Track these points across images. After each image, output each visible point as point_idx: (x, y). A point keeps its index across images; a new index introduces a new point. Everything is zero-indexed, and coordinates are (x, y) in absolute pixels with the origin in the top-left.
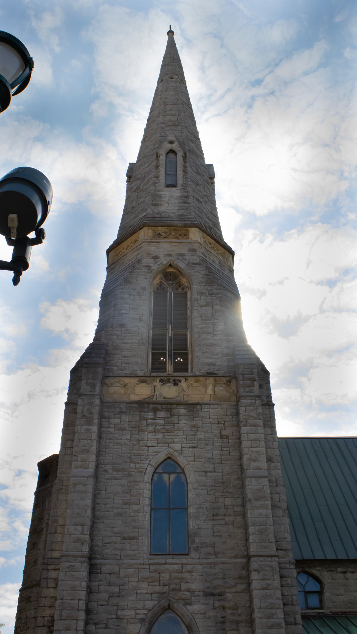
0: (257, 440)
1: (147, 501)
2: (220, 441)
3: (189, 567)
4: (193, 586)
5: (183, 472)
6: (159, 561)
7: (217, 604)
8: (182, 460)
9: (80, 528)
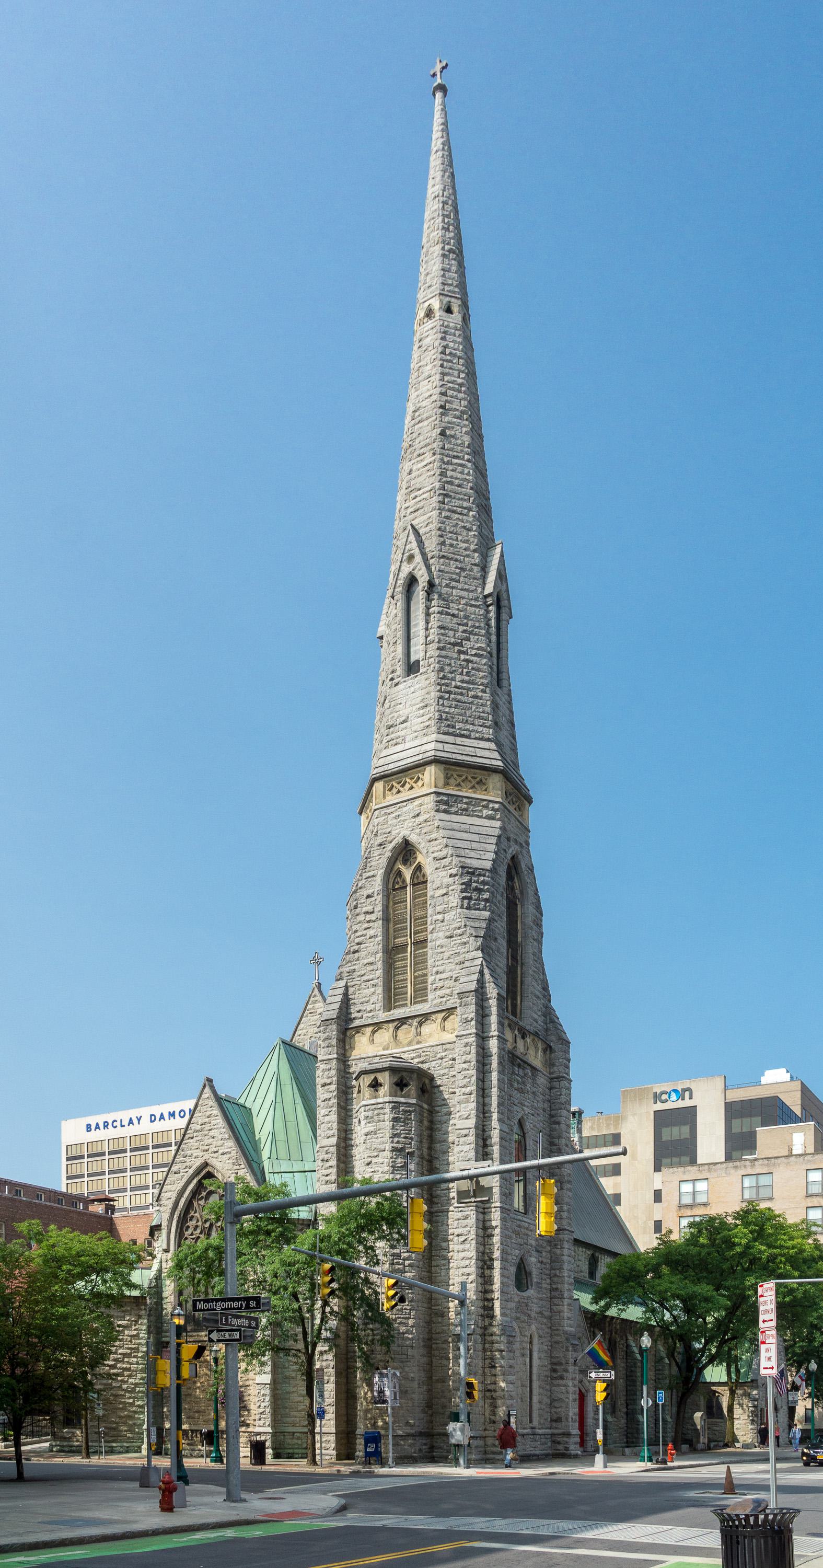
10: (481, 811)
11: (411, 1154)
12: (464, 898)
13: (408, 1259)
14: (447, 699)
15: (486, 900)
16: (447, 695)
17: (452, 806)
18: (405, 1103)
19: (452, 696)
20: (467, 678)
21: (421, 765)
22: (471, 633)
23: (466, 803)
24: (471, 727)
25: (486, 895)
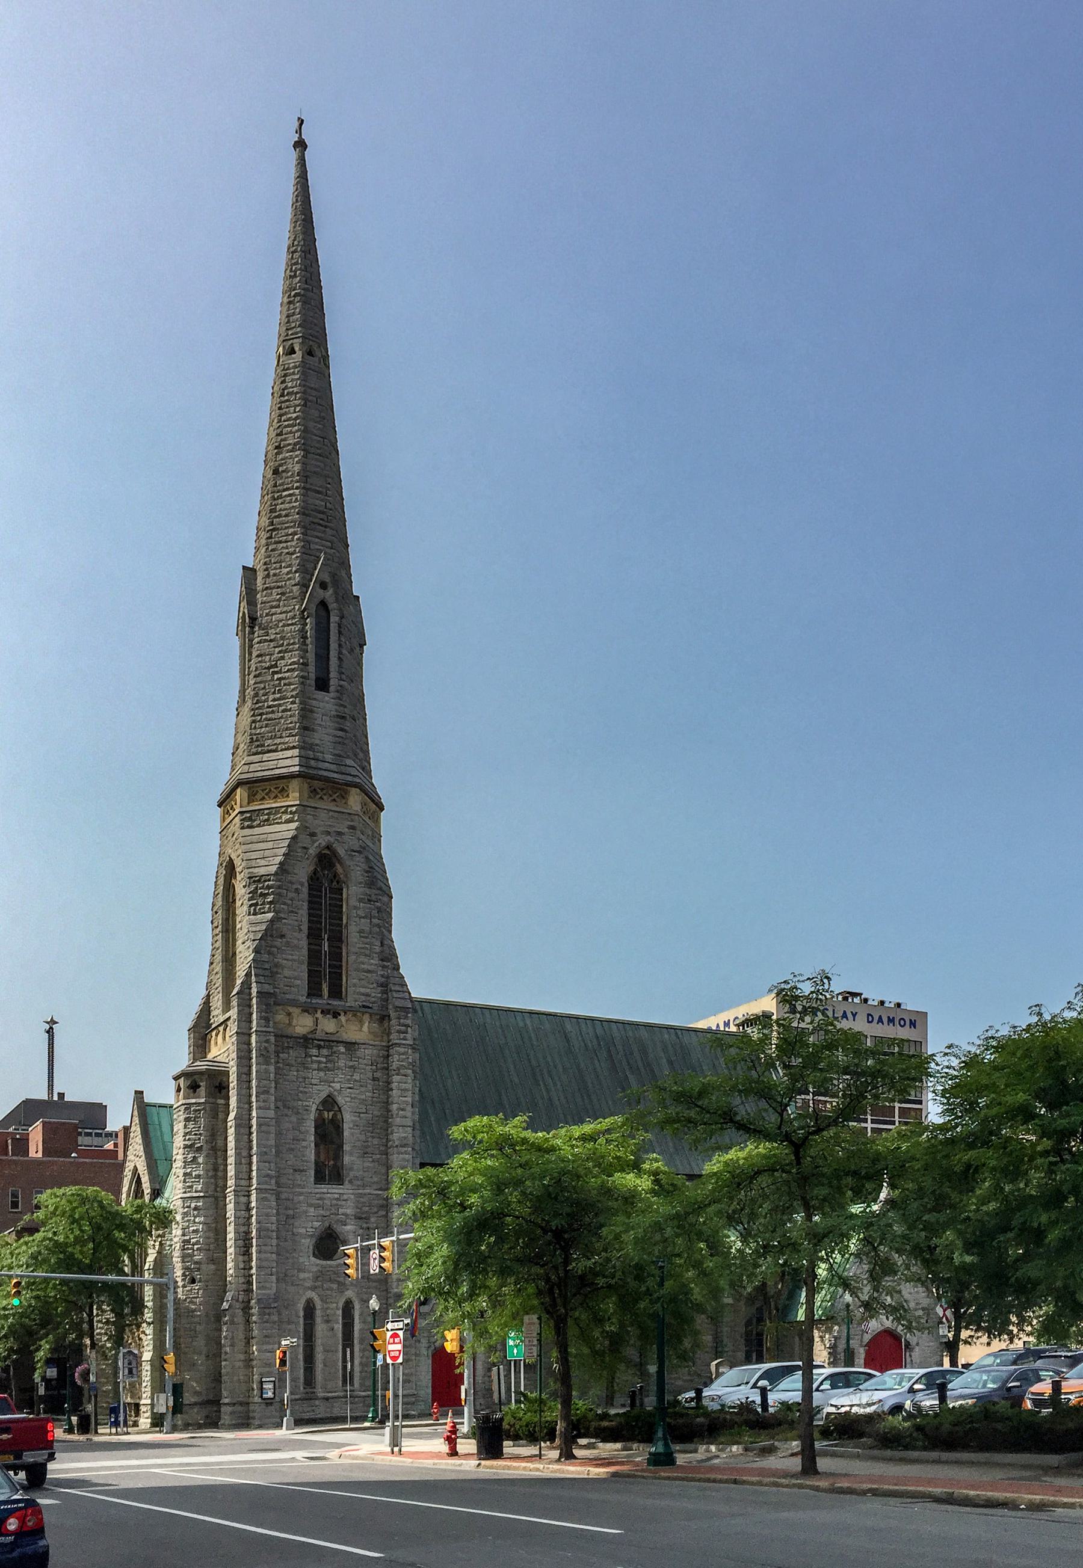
0: (406, 1090)
1: (313, 1138)
2: (372, 1082)
3: (345, 1197)
4: (349, 1211)
5: (340, 1111)
6: (323, 1190)
7: (365, 1225)
8: (340, 1100)
9: (267, 1164)
10: (281, 818)
11: (199, 1149)
12: (251, 906)
13: (197, 1243)
14: (259, 721)
15: (270, 903)
16: (259, 717)
17: (255, 820)
18: (195, 1103)
19: (264, 717)
20: (278, 696)
21: (233, 790)
22: (286, 651)
23: (267, 814)
24: (278, 741)
25: (270, 898)
